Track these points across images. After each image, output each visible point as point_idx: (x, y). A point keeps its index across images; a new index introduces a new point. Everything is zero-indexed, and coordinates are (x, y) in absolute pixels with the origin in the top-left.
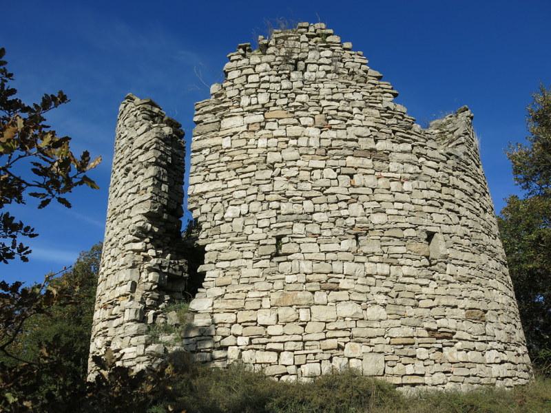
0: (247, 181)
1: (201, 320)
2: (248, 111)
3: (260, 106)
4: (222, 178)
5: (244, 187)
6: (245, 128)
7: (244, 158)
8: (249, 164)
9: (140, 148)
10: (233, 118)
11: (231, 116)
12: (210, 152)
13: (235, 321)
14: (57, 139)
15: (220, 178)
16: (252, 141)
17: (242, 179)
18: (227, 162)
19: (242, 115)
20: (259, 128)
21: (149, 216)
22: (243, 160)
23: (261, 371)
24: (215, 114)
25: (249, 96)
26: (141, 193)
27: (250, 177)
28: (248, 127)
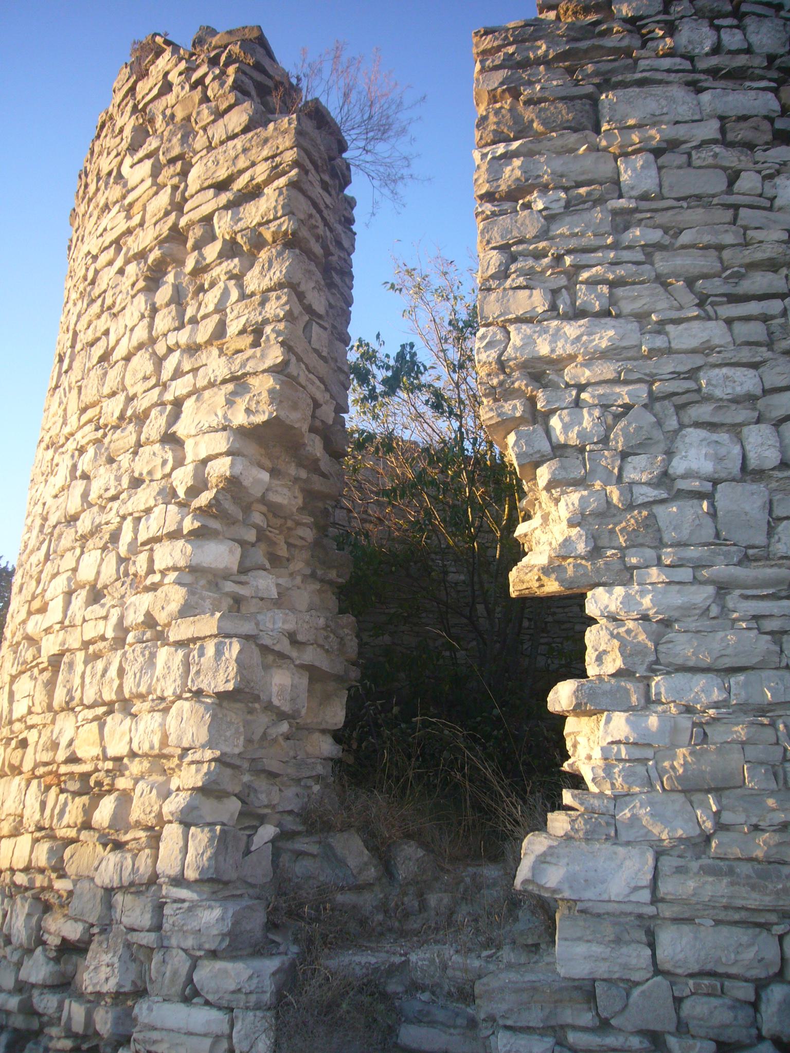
0: (756, 330)
1: (596, 949)
2: (714, 73)
3: (759, 62)
4: (637, 306)
5: (745, 355)
6: (711, 129)
7: (729, 239)
8: (753, 266)
9: (221, 186)
10: (658, 90)
11: (641, 83)
12: (568, 205)
13: (776, 969)
14: (29, 673)
15: (627, 307)
16: (749, 182)
17: (729, 322)
18: (650, 250)
19: (688, 84)
20: (768, 137)
21: (253, 439)
22: (720, 248)
23: (688, 1032)
24: (570, 71)
25: (711, 20)
26: (233, 346)
27: (765, 318)
28: (723, 130)
